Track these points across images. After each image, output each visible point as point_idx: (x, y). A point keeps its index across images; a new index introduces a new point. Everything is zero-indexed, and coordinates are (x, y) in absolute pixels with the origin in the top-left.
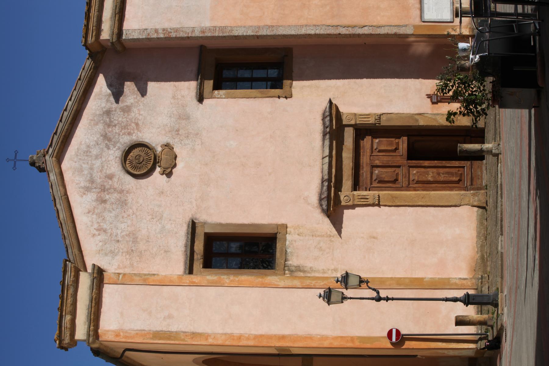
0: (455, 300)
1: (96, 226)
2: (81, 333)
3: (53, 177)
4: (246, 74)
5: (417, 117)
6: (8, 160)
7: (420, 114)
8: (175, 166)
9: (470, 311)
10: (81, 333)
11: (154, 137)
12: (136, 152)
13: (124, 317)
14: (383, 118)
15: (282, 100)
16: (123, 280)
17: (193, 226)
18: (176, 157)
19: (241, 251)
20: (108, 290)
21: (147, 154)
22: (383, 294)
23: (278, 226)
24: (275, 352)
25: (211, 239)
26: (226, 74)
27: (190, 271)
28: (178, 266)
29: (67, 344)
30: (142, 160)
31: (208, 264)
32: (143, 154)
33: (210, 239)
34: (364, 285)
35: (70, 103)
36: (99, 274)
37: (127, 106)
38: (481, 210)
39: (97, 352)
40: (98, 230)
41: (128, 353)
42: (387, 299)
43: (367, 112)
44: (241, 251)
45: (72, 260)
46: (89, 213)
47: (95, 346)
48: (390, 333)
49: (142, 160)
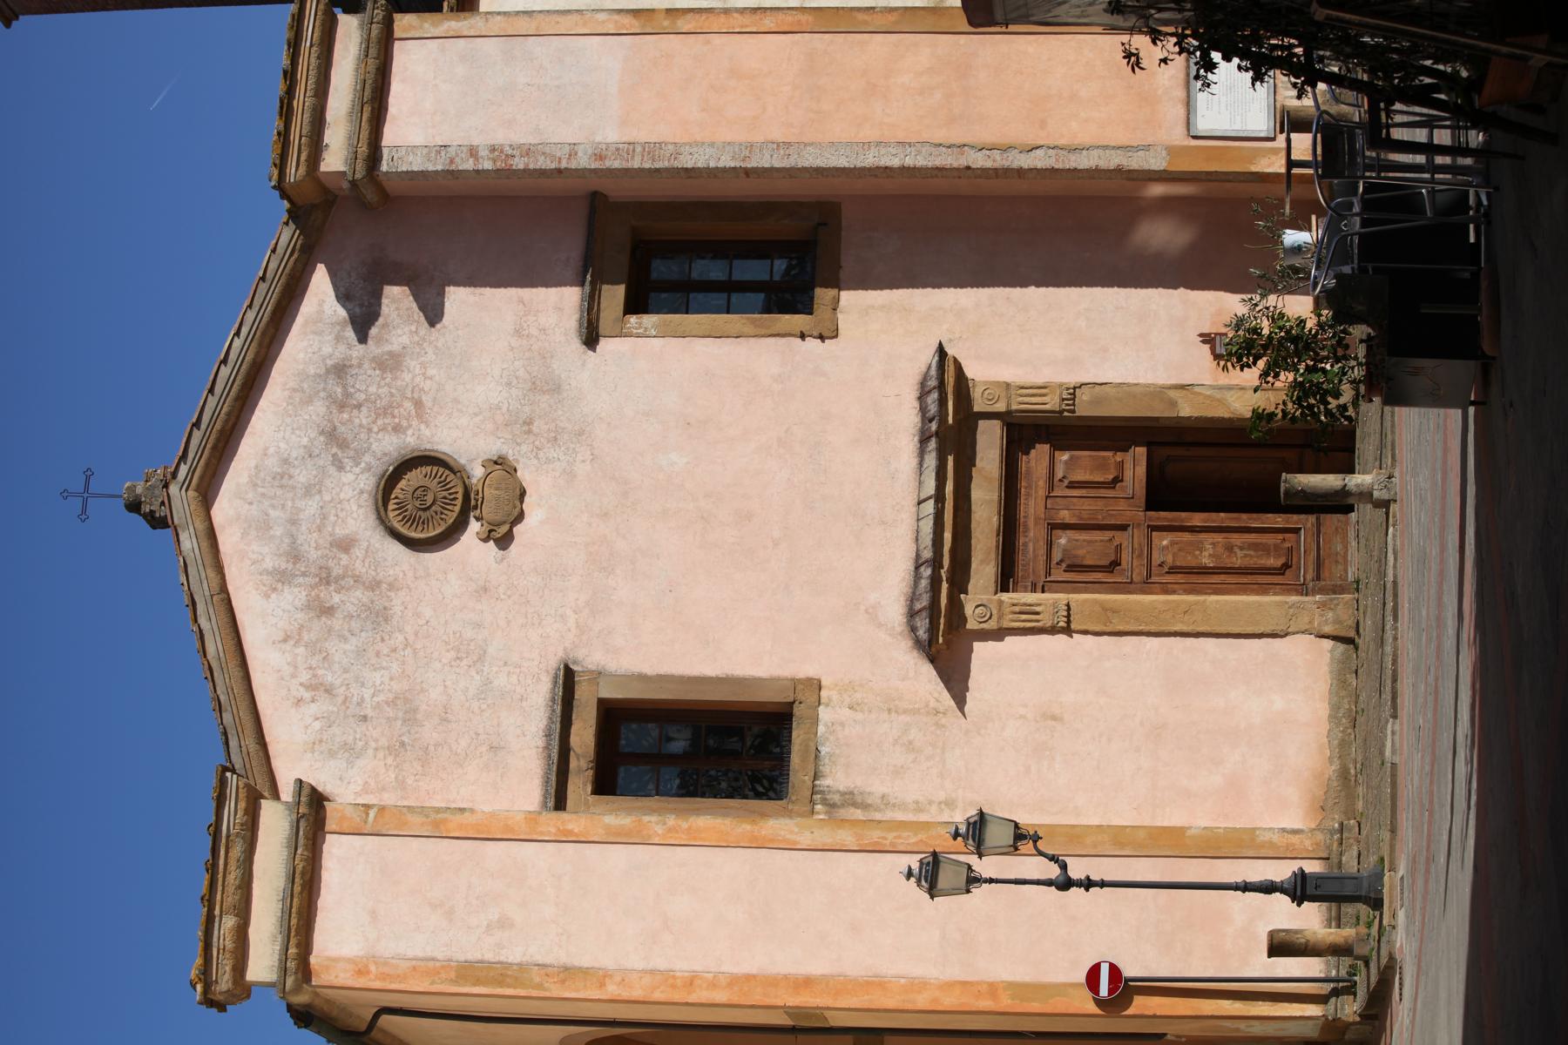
0: (1268, 888)
1: (305, 677)
2: (262, 964)
3: (188, 543)
4: (713, 270)
5: (1173, 394)
6: (66, 495)
7: (1182, 387)
8: (520, 517)
9: (1309, 919)
10: (262, 964)
11: (465, 439)
12: (414, 478)
13: (379, 923)
14: (1084, 396)
15: (812, 344)
16: (378, 823)
17: (568, 679)
18: (523, 493)
19: (699, 750)
20: (335, 849)
21: (444, 484)
22: (1076, 872)
23: (795, 683)
24: (785, 1021)
25: (615, 717)
26: (662, 269)
27: (560, 802)
28: (523, 785)
29: (222, 995)
30: (433, 502)
31: (605, 784)
32: (433, 485)
33: (613, 715)
34: (1027, 847)
35: (238, 343)
36: (313, 809)
37: (391, 354)
38: (1341, 647)
39: (304, 1017)
40: (309, 687)
41: (385, 1020)
42: (1088, 884)
43: (1039, 380)
44: (699, 750)
45: (239, 769)
46: (285, 641)
47: (300, 999)
48: (1093, 975)
49: (433, 502)
